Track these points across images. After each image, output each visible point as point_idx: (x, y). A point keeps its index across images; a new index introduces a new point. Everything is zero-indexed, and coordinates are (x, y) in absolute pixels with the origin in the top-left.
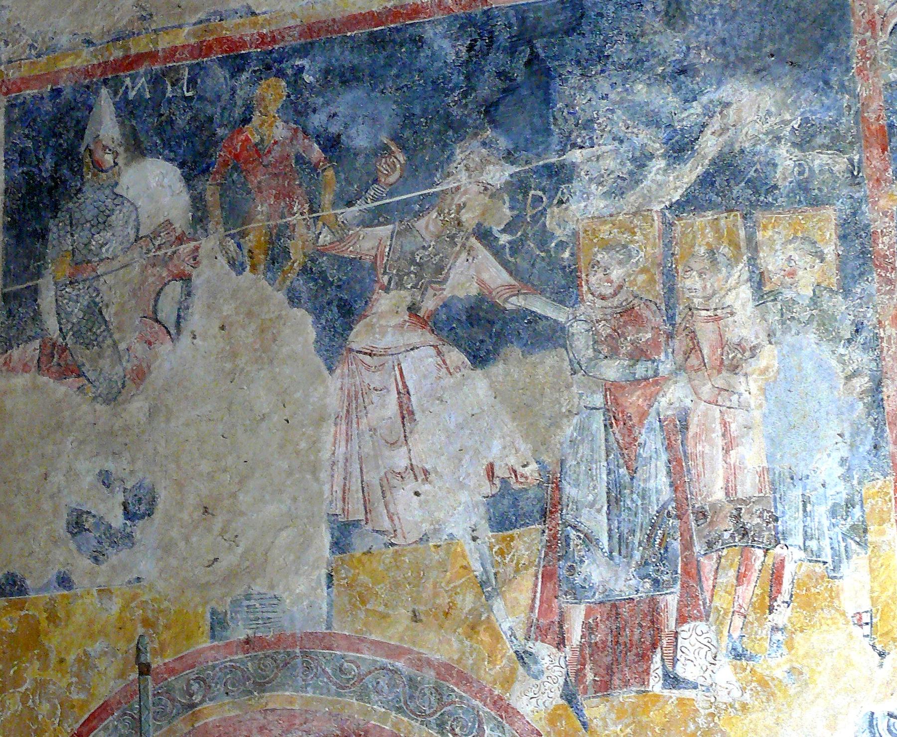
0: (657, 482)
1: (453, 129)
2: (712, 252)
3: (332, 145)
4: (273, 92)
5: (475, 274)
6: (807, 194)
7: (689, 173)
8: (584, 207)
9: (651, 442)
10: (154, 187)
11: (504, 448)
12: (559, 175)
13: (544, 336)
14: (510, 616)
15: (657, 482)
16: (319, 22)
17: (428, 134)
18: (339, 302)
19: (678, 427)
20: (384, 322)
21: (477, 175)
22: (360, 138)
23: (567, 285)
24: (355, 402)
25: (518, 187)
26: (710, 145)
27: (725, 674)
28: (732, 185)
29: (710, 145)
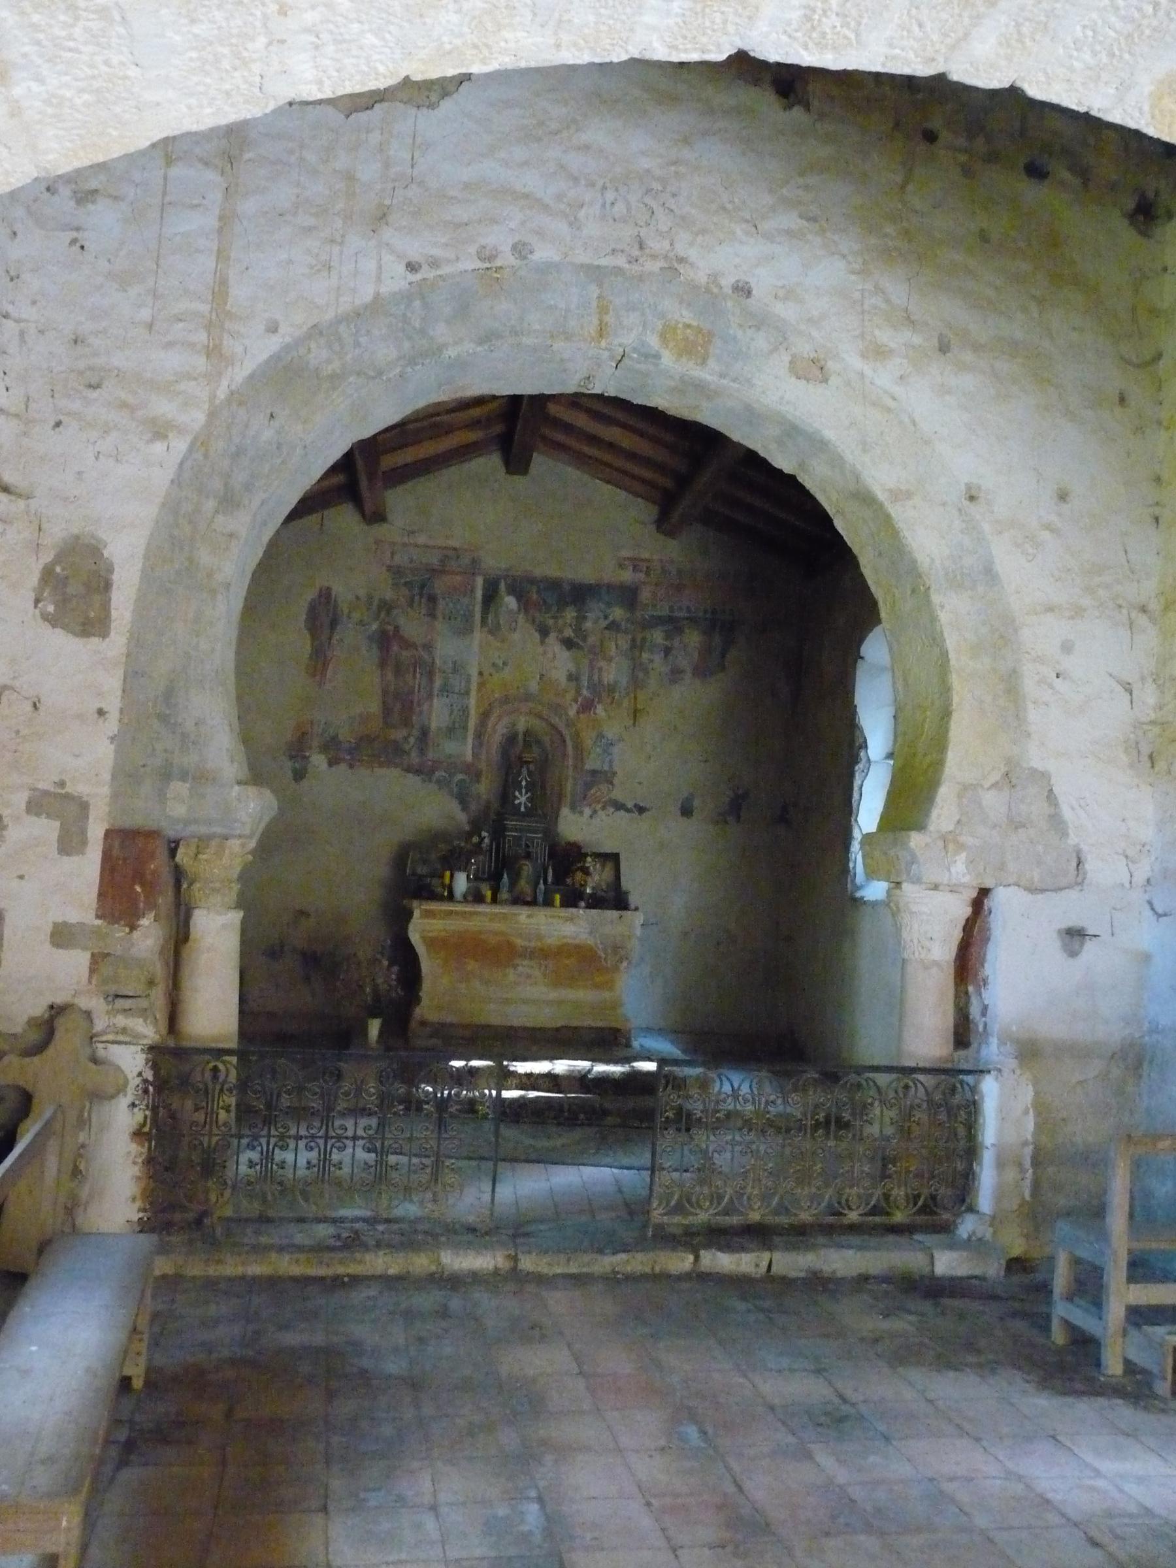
0: (596, 678)
1: (567, 604)
2: (461, 35)
3: (545, 602)
4: (534, 589)
5: (568, 633)
6: (626, 632)
7: (607, 622)
8: (588, 625)
9: (596, 671)
10: (511, 602)
11: (300, 1358)
12: (585, 618)
13: (579, 647)
14: (569, 697)
15: (596, 678)
16: (181, 464)
17: (562, 604)
18: (544, 632)
19: (600, 669)
20: (552, 638)
21: (570, 614)
22: (549, 601)
23: (584, 638)
24: (545, 653)
25: (577, 617)
26: (611, 618)
27: (603, 714)
28: (613, 626)
29: (611, 618)
